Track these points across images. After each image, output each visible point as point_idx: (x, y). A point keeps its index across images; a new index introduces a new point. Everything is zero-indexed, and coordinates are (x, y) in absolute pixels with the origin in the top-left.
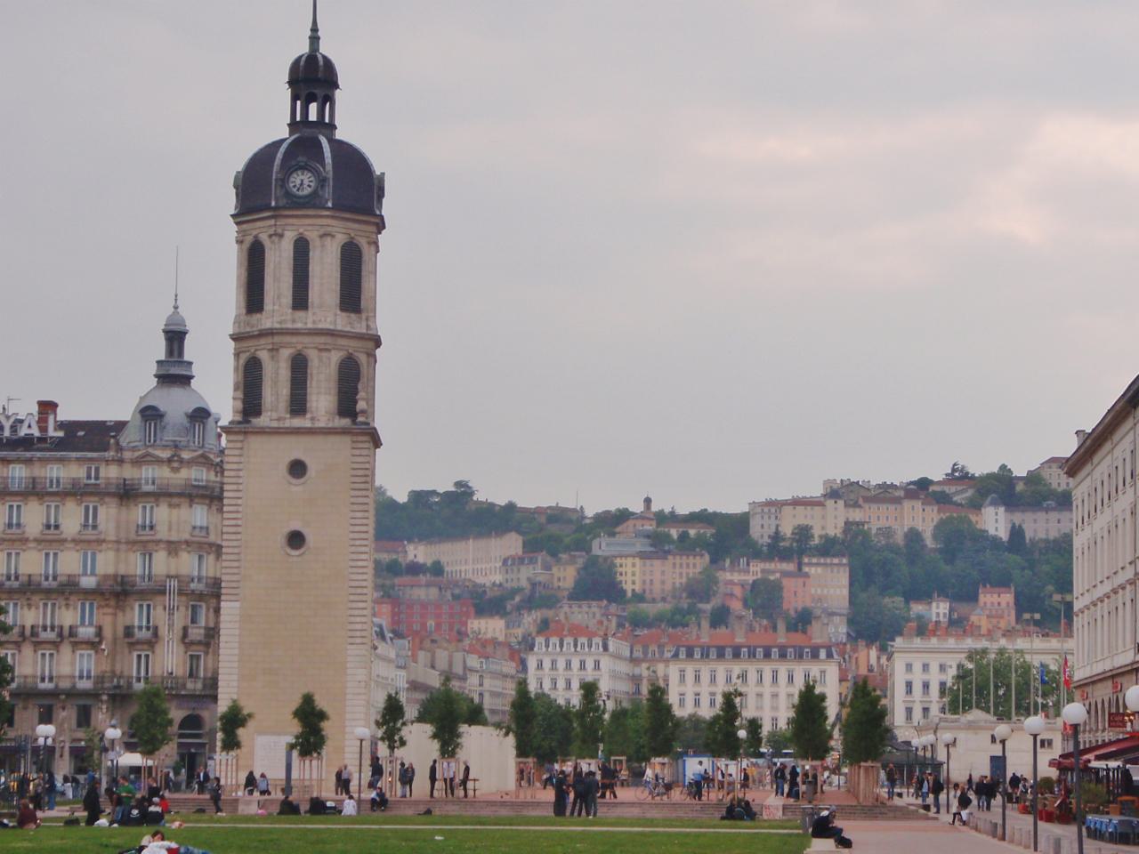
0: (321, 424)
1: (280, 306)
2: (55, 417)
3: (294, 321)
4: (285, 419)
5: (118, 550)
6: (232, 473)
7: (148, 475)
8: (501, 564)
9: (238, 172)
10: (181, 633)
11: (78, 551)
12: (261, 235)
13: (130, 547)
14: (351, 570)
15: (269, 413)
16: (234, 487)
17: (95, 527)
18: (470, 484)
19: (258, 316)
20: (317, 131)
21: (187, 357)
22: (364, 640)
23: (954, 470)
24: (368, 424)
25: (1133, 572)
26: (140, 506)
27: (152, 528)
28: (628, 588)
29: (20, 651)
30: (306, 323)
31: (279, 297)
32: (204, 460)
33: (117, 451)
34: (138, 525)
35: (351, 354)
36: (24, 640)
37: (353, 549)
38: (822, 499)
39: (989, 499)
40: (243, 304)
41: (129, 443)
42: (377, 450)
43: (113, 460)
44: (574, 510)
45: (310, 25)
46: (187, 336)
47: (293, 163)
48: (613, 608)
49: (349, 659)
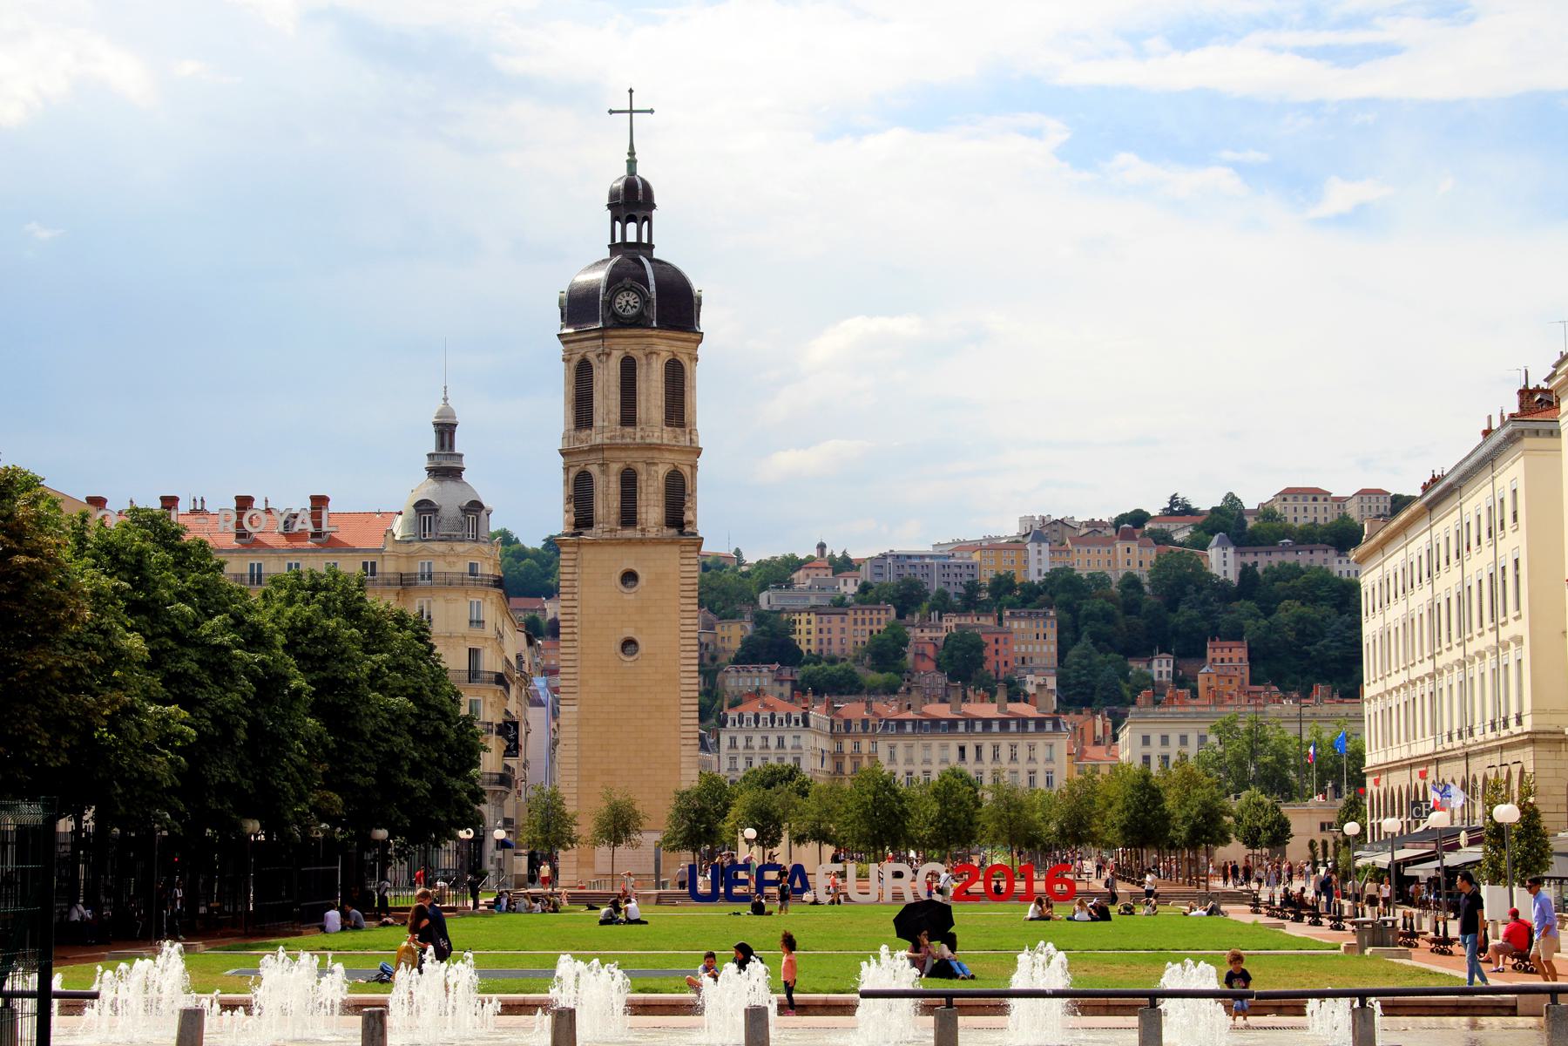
0: (652, 535)
3: (623, 437)
4: (616, 530)
6: (567, 583)
12: (588, 354)
15: (601, 525)
16: (570, 597)
19: (588, 432)
21: (457, 450)
28: (804, 647)
39: (1216, 537)
40: (571, 420)
45: (628, 151)
46: (457, 429)
47: (619, 285)
48: (786, 672)
49: (683, 759)
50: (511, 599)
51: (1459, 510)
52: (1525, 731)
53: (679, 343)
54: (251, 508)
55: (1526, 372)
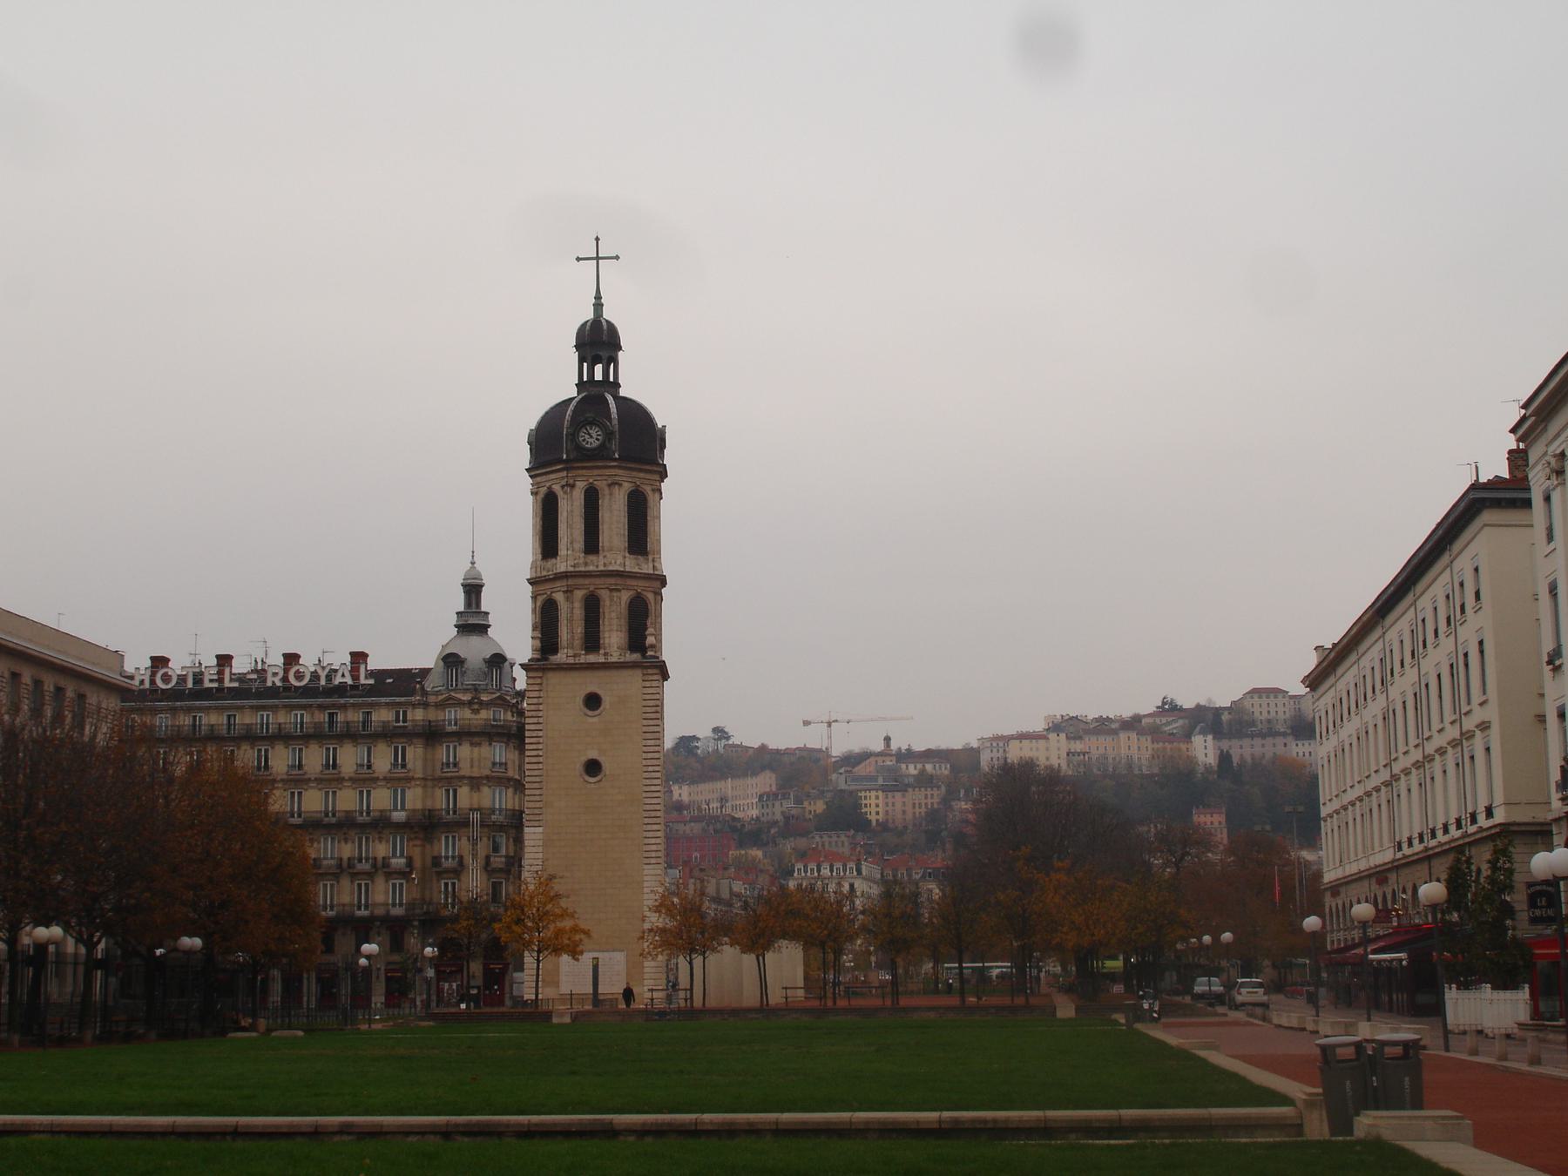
0: (614, 659)
1: (573, 550)
2: (366, 667)
3: (586, 564)
5: (424, 787)
7: (454, 717)
8: (757, 800)
9: (531, 430)
10: (483, 862)
11: (388, 788)
12: (553, 486)
13: (436, 783)
14: (644, 795)
16: (535, 720)
17: (404, 766)
18: (726, 730)
19: (554, 561)
20: (603, 389)
22: (659, 861)
23: (1164, 703)
24: (658, 658)
25: (1389, 774)
26: (444, 745)
27: (455, 765)
28: (873, 818)
29: (338, 882)
30: (597, 566)
31: (572, 543)
32: (501, 702)
33: (422, 696)
34: (443, 764)
35: (640, 593)
36: (341, 872)
37: (646, 775)
38: (1045, 733)
40: (539, 551)
41: (433, 687)
42: (665, 683)
43: (419, 704)
44: (820, 750)
48: (859, 837)
50: (300, 663)
51: (1413, 607)
52: (1496, 823)
53: (642, 475)
54: (297, 663)
55: (1477, 467)
